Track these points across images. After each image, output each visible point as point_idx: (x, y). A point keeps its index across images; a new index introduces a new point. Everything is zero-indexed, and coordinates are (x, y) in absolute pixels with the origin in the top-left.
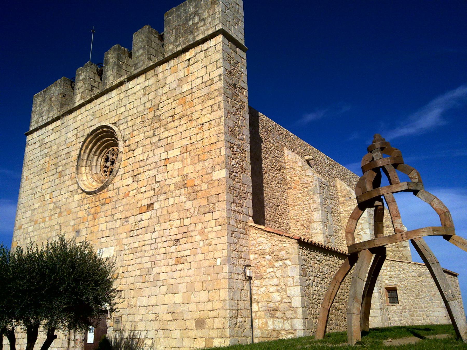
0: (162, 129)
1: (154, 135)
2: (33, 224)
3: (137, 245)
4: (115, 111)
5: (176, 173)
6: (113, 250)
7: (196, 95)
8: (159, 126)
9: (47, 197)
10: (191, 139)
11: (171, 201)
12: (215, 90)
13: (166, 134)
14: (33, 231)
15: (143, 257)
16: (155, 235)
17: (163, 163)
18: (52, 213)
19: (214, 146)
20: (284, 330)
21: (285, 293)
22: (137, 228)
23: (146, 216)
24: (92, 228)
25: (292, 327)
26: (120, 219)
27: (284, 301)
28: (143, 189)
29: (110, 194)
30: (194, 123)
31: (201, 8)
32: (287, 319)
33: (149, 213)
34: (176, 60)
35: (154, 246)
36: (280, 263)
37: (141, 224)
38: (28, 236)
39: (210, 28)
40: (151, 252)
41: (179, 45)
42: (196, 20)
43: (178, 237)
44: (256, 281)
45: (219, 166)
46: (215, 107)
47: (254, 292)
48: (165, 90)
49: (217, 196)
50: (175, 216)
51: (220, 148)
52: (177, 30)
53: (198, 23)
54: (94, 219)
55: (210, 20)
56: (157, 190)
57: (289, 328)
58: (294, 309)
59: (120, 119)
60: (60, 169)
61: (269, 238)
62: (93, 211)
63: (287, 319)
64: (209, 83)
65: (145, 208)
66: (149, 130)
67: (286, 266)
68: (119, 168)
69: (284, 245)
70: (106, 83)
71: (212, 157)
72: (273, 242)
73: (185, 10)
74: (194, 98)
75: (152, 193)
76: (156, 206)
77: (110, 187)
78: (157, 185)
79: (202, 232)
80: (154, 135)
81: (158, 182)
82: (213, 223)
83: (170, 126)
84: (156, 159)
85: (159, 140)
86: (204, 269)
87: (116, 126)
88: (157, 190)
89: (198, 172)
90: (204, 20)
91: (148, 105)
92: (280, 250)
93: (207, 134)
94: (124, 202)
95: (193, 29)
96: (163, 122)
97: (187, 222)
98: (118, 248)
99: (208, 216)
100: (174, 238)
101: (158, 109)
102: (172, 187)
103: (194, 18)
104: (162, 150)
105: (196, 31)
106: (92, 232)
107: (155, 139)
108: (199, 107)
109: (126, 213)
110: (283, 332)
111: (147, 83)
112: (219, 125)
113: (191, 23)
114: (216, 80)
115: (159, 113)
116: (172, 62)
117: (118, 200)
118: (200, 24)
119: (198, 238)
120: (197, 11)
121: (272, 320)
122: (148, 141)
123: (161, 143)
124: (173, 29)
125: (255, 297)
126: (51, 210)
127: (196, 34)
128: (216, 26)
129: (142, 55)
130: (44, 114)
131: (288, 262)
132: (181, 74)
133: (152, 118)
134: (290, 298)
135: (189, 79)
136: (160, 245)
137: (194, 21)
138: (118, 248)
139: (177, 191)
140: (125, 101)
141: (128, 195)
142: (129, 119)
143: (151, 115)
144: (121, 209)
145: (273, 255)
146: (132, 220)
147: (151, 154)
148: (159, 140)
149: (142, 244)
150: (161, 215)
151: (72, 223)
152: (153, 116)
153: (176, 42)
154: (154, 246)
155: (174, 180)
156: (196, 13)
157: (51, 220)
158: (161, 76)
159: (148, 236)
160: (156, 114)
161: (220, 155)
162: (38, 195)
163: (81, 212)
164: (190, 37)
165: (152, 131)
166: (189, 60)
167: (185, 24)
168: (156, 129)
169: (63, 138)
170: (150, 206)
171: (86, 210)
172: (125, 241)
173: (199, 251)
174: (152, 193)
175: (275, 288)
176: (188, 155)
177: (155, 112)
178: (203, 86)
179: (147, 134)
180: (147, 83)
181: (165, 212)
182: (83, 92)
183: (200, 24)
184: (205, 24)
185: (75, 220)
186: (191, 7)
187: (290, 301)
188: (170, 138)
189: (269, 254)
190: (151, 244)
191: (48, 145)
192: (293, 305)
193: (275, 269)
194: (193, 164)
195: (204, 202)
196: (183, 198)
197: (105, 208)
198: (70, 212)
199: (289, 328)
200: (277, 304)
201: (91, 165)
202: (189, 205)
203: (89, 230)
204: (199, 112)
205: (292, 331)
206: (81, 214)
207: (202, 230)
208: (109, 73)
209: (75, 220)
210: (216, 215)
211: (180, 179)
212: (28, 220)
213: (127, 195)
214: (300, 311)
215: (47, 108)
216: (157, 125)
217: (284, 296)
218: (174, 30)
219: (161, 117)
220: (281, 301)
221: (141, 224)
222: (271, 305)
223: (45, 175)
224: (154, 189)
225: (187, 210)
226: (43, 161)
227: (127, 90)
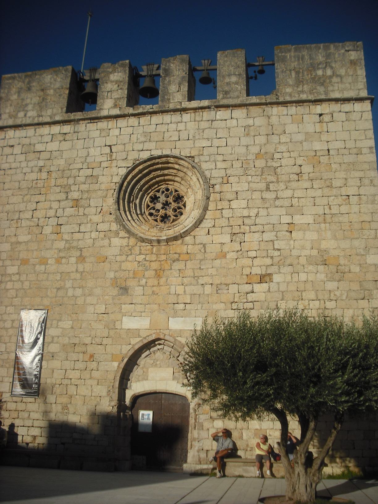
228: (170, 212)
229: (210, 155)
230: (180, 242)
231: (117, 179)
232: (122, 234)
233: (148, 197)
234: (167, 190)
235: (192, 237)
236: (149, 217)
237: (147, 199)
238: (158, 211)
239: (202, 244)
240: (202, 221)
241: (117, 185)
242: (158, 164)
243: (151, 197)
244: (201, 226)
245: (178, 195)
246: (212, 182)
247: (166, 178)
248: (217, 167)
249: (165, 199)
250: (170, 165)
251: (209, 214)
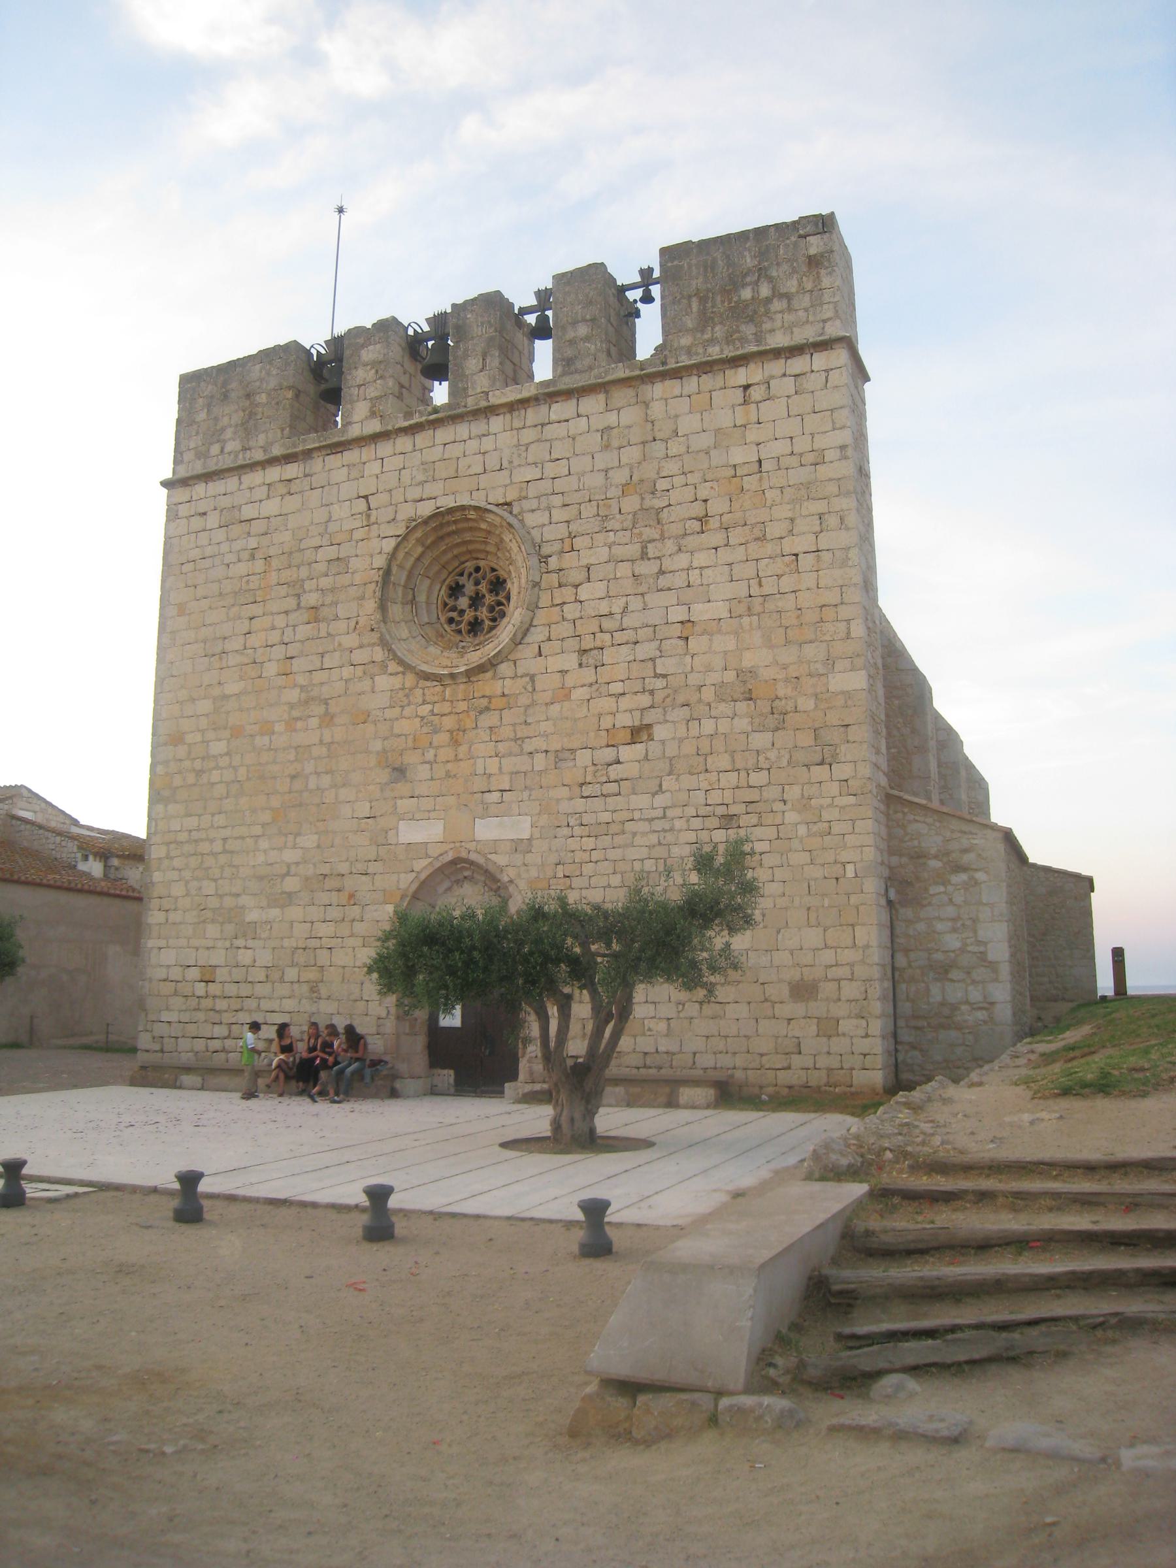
0: (670, 546)
1: (644, 556)
2: (226, 734)
3: (606, 817)
4: (506, 473)
5: (718, 662)
6: (528, 825)
7: (778, 479)
8: (658, 537)
9: (271, 669)
10: (760, 585)
11: (708, 726)
12: (830, 480)
13: (682, 560)
14: (228, 754)
15: (626, 846)
16: (660, 800)
17: (677, 630)
18: (295, 714)
19: (829, 613)
20: (967, 1002)
21: (971, 935)
22: (604, 779)
23: (626, 752)
24: (449, 766)
25: (985, 997)
26: (547, 752)
27: (969, 948)
28: (617, 688)
29: (497, 687)
30: (770, 548)
31: (778, 264)
32: (974, 982)
33: (639, 748)
34: (708, 381)
35: (658, 825)
36: (963, 877)
37: (615, 772)
38: (212, 764)
39: (807, 322)
40: (653, 839)
41: (712, 341)
42: (765, 291)
43: (733, 810)
44: (902, 911)
45: (847, 663)
46: (833, 521)
47: (898, 931)
48: (675, 448)
49: (842, 729)
50: (724, 762)
51: (848, 621)
52: (703, 300)
53: (768, 301)
54: (456, 743)
55: (806, 300)
56: (659, 696)
57: (980, 998)
58: (993, 966)
59: (526, 498)
60: (312, 599)
61: (938, 824)
62: (449, 722)
63: (974, 982)
64: (810, 458)
65: (626, 736)
66: (625, 541)
67: (977, 883)
68: (531, 625)
69: (975, 842)
70: (465, 389)
71: (828, 638)
72: (948, 834)
73: (728, 257)
74: (765, 485)
75: (645, 700)
76: (660, 732)
77: (505, 669)
78: (660, 683)
79: (804, 804)
80: (644, 556)
81: (664, 676)
82: (834, 788)
83: (691, 542)
84: (655, 617)
85: (662, 572)
86: (812, 883)
87: (511, 513)
88: (659, 696)
89: (785, 667)
90: (788, 297)
91: (620, 477)
92: (965, 851)
93: (808, 580)
94: (555, 709)
95: (755, 312)
96: (676, 529)
97: (757, 778)
98: (544, 820)
99: (820, 772)
100: (721, 810)
101: (653, 493)
102: (708, 694)
103: (757, 283)
104: (671, 598)
105: (765, 319)
106: (448, 775)
107: (644, 568)
108: (784, 512)
109: (565, 740)
110: (964, 1007)
111: (612, 418)
112: (844, 563)
113: (747, 294)
114: (830, 455)
115: (658, 503)
116: (692, 384)
117: (533, 704)
118: (777, 305)
119: (791, 817)
120: (766, 269)
121: (939, 984)
122: (624, 570)
123: (663, 582)
124: (690, 297)
125: (901, 940)
126: (292, 706)
127: (767, 326)
128: (824, 321)
129: (587, 339)
130: (229, 433)
131: (980, 876)
132: (724, 419)
133: (635, 514)
134: (985, 944)
135: (752, 435)
136: (679, 824)
137: (756, 291)
138: (544, 820)
139: (723, 704)
140: (537, 452)
141: (567, 697)
142: (557, 500)
143: (631, 504)
144: (545, 727)
145: (945, 860)
146: (584, 758)
147: (635, 603)
148: (662, 572)
149: (626, 815)
150: (679, 757)
151: (378, 745)
152: (638, 507)
153: (703, 332)
154: (658, 825)
155: (714, 678)
156: (762, 272)
157: (295, 730)
158: (657, 410)
159: (641, 801)
160: (648, 503)
161: (848, 636)
162: (233, 659)
163: (404, 722)
164: (748, 330)
165: (638, 547)
166: (746, 387)
167: (729, 292)
168: (650, 542)
169: (320, 516)
170: (638, 733)
171: (422, 718)
172: (565, 807)
173: (795, 844)
174: (645, 700)
175: (950, 924)
176: (755, 623)
177: (643, 499)
178: (794, 461)
179: (617, 550)
180: (612, 418)
181: (689, 748)
182: (377, 398)
183: (777, 305)
184: (790, 309)
185: (385, 739)
186: (746, 253)
187: (982, 949)
188: (697, 571)
189: (936, 857)
190: (651, 820)
191: (258, 527)
192: (990, 957)
193: (950, 888)
194: (772, 647)
195: (805, 739)
196: (742, 724)
197: (487, 720)
198: (365, 717)
199: (980, 998)
200: (952, 955)
201: (413, 601)
202: (760, 740)
203: (440, 771)
204: (785, 525)
205: (986, 1005)
206: (404, 726)
207: (805, 802)
208: (472, 364)
209: (385, 739)
210: (842, 771)
211: (730, 676)
212: (204, 723)
213: (564, 694)
214: (1005, 970)
215: (237, 418)
216: (653, 533)
217: (969, 941)
218: (694, 299)
219: (664, 515)
220: (963, 950)
221: (615, 772)
222: (939, 956)
223: (256, 610)
224: (652, 692)
225: (758, 751)
226: (242, 569)
227: (543, 425)
228: (483, 613)
229: (538, 497)
230: (489, 675)
231: (380, 562)
232: (393, 667)
233: (444, 588)
234: (478, 569)
235: (511, 664)
236: (446, 626)
237: (442, 592)
238: (462, 612)
239: (527, 675)
240: (528, 630)
241: (381, 572)
242: (448, 523)
243: (451, 588)
244: (527, 640)
245: (498, 578)
246: (546, 550)
247: (471, 547)
248: (553, 520)
249: (473, 588)
250: (471, 524)
251: (541, 617)
